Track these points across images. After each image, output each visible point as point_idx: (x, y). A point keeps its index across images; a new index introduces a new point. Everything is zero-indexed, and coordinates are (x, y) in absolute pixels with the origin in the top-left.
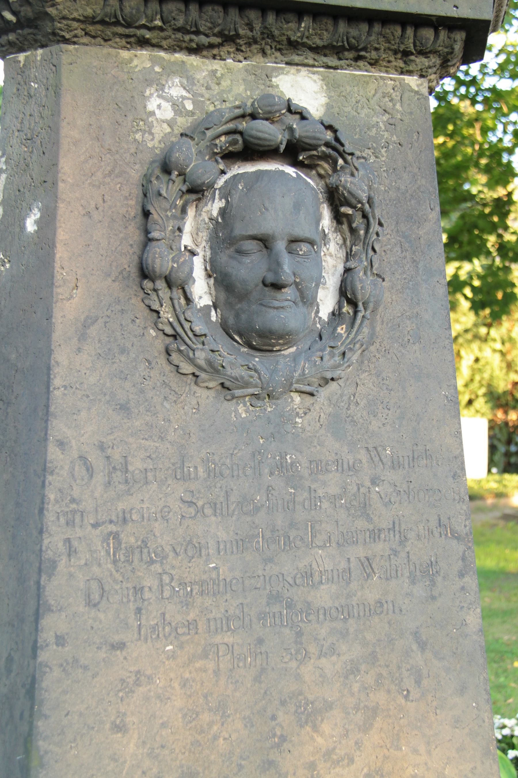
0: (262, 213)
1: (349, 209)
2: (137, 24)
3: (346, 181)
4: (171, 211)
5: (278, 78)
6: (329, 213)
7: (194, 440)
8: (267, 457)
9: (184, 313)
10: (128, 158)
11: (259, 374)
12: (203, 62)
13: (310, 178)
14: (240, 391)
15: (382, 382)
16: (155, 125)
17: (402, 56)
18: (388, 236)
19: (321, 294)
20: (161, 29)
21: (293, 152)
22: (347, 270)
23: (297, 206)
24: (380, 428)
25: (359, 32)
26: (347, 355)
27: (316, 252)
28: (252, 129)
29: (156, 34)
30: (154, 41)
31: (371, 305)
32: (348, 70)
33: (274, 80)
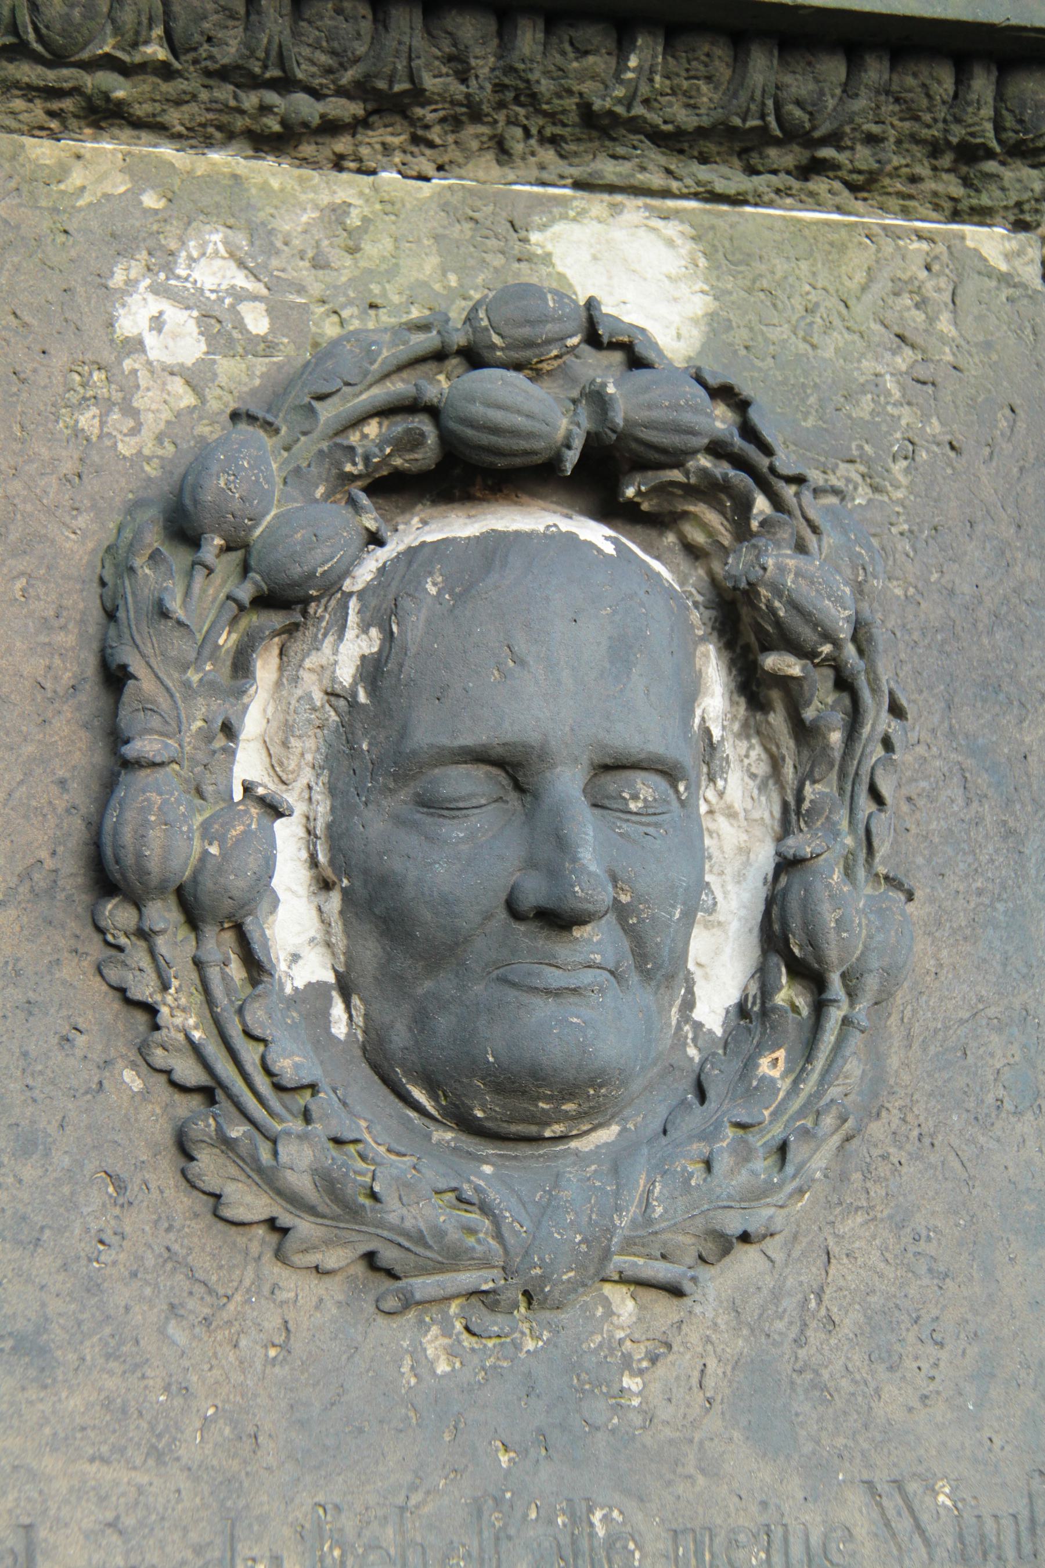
0: (504, 675)
1: (791, 659)
2: (85, 55)
3: (782, 569)
4: (198, 669)
5: (549, 233)
6: (724, 672)
7: (271, 1460)
8: (525, 1516)
9: (240, 1011)
10: (52, 492)
11: (497, 1222)
12: (301, 180)
13: (657, 558)
14: (430, 1280)
15: (912, 1249)
16: (143, 383)
17: (955, 161)
18: (921, 750)
19: (701, 945)
20: (165, 71)
21: (605, 474)
22: (787, 865)
23: (622, 651)
24: (910, 1410)
25: (816, 84)
26: (795, 1154)
27: (683, 804)
28: (472, 400)
29: (146, 87)
30: (140, 111)
31: (871, 983)
32: (780, 208)
33: (535, 237)
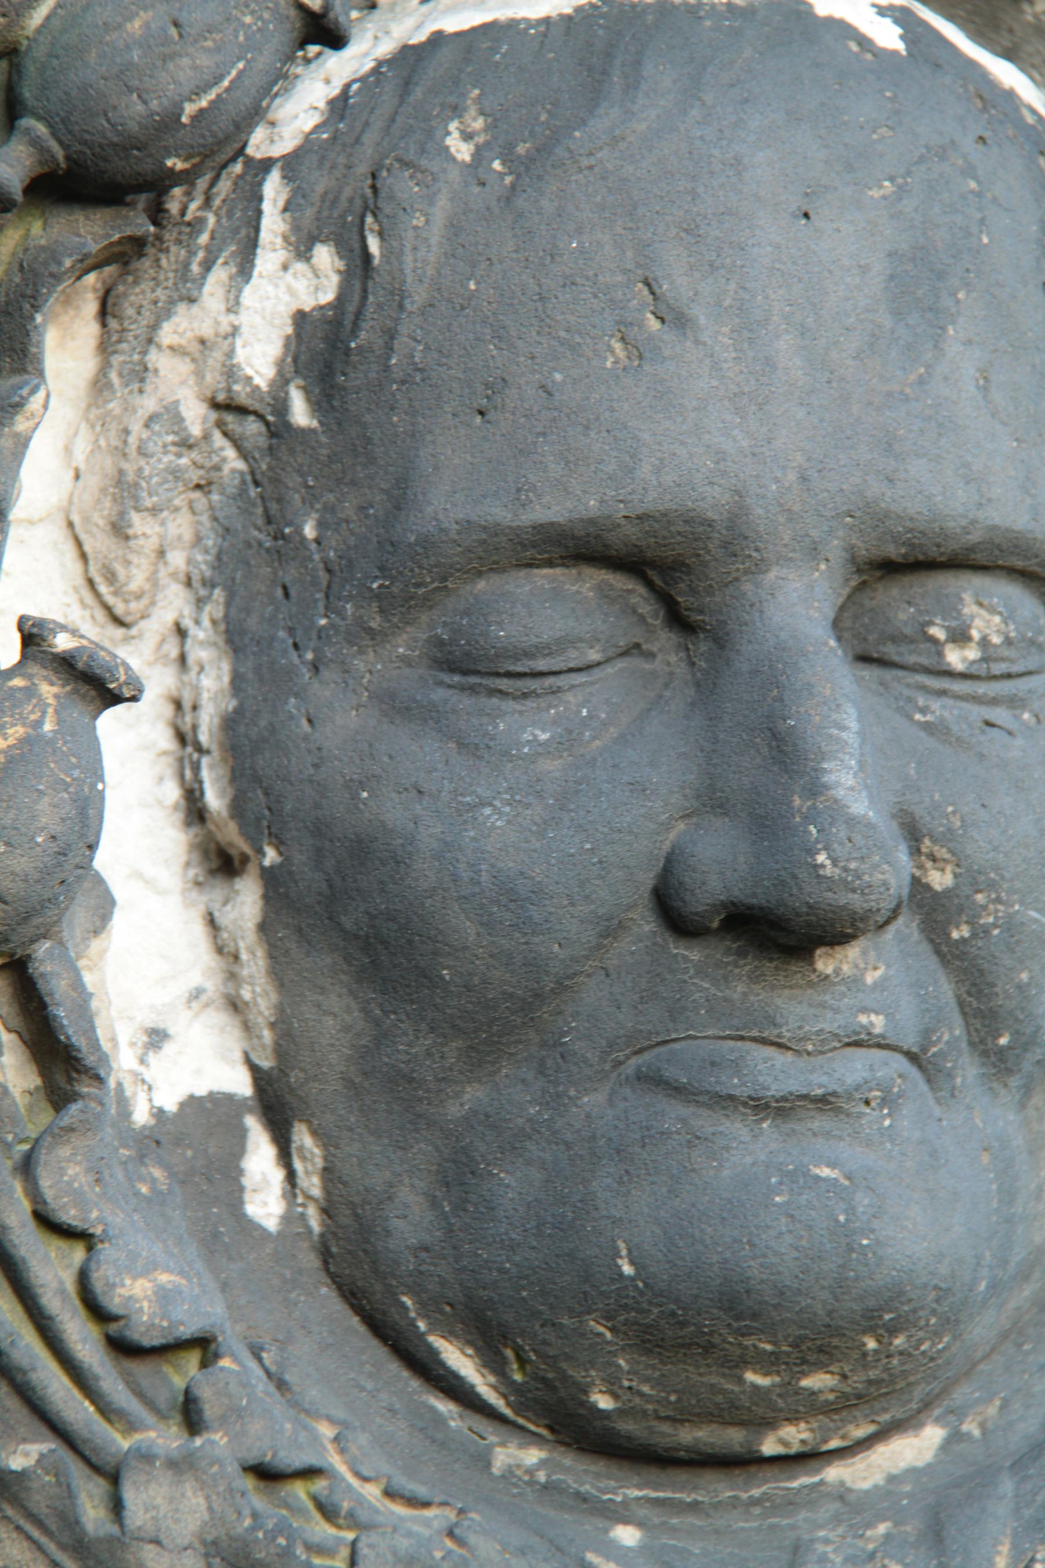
0: (640, 352)
13: (1009, 54)
